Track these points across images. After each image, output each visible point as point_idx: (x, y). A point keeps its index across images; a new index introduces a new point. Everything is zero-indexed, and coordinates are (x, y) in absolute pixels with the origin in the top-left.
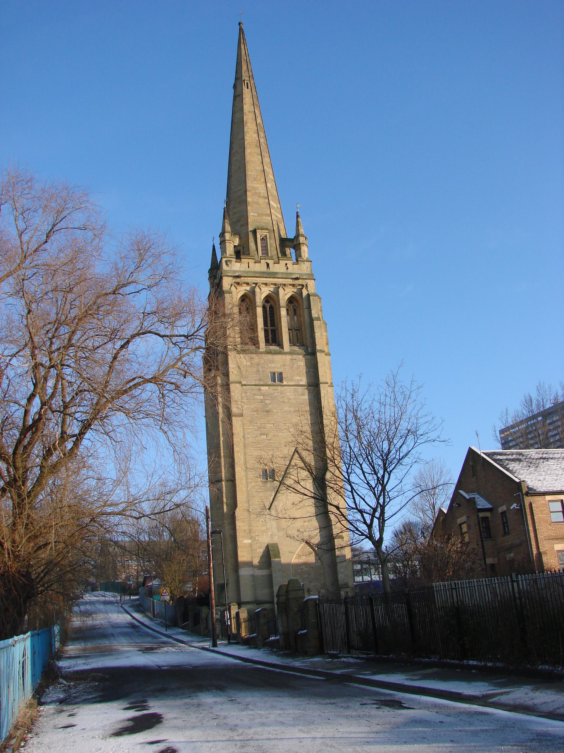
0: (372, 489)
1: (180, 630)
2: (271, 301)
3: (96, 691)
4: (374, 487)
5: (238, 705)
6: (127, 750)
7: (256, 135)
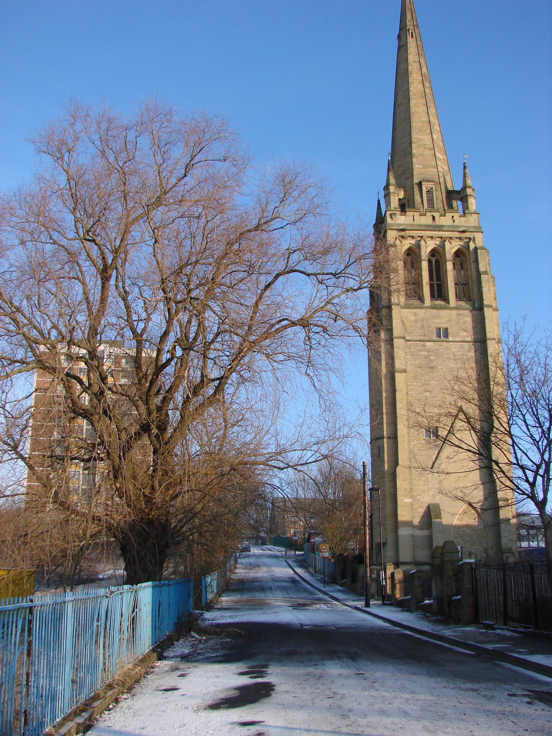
0: (536, 443)
1: (339, 587)
2: (437, 255)
3: (223, 648)
4: (537, 440)
5: (364, 681)
6: (211, 732)
7: (421, 86)
